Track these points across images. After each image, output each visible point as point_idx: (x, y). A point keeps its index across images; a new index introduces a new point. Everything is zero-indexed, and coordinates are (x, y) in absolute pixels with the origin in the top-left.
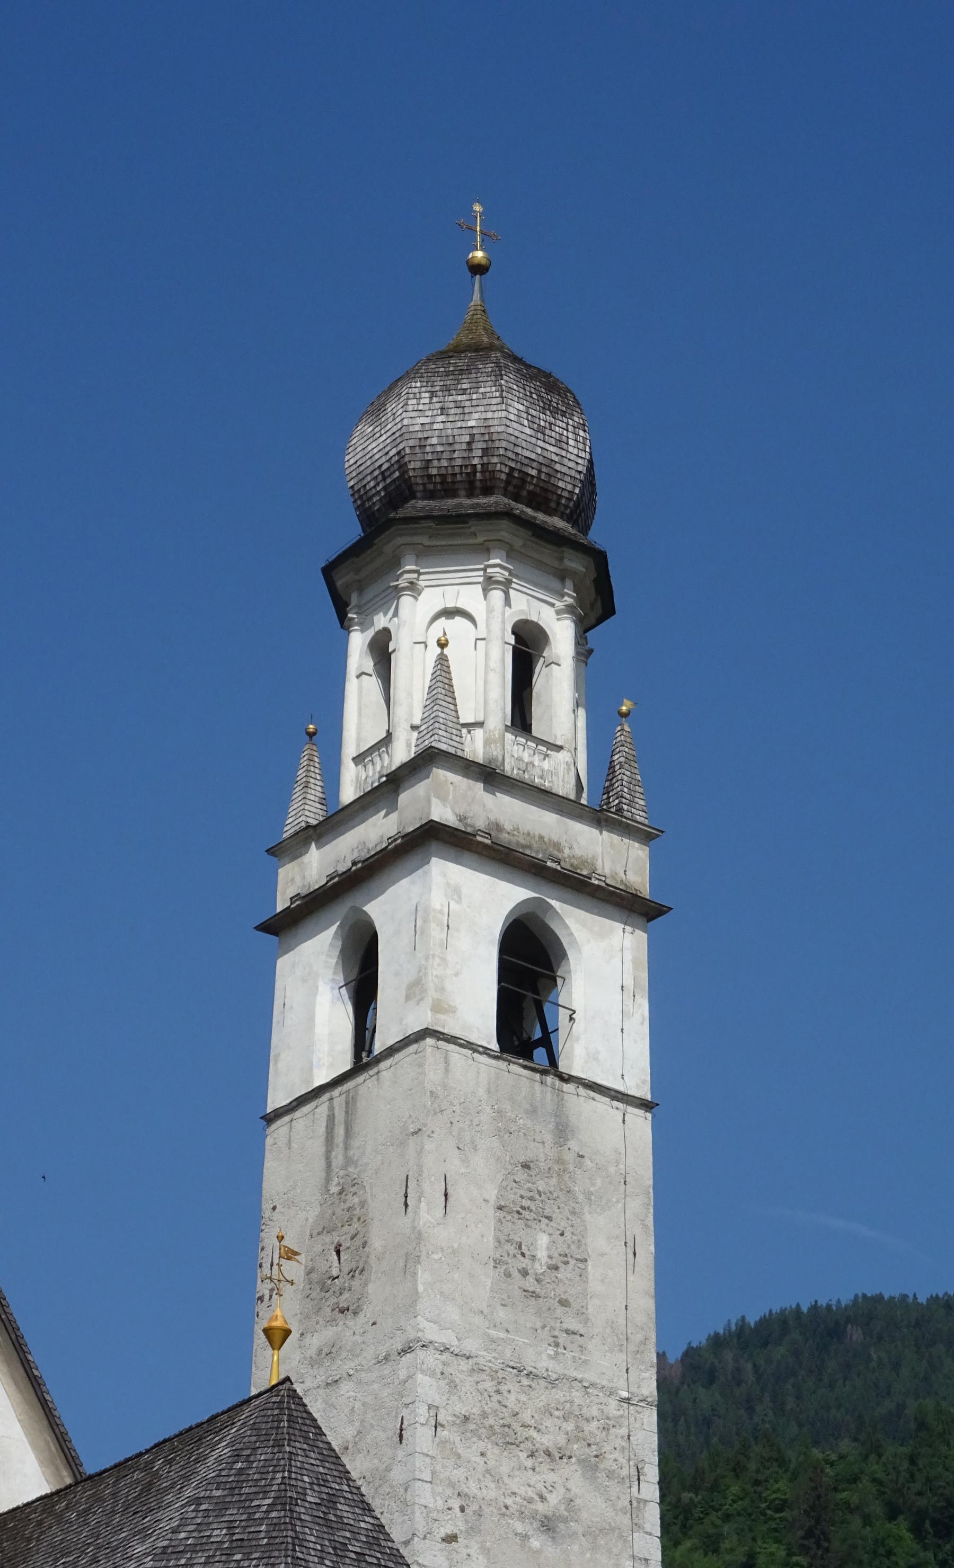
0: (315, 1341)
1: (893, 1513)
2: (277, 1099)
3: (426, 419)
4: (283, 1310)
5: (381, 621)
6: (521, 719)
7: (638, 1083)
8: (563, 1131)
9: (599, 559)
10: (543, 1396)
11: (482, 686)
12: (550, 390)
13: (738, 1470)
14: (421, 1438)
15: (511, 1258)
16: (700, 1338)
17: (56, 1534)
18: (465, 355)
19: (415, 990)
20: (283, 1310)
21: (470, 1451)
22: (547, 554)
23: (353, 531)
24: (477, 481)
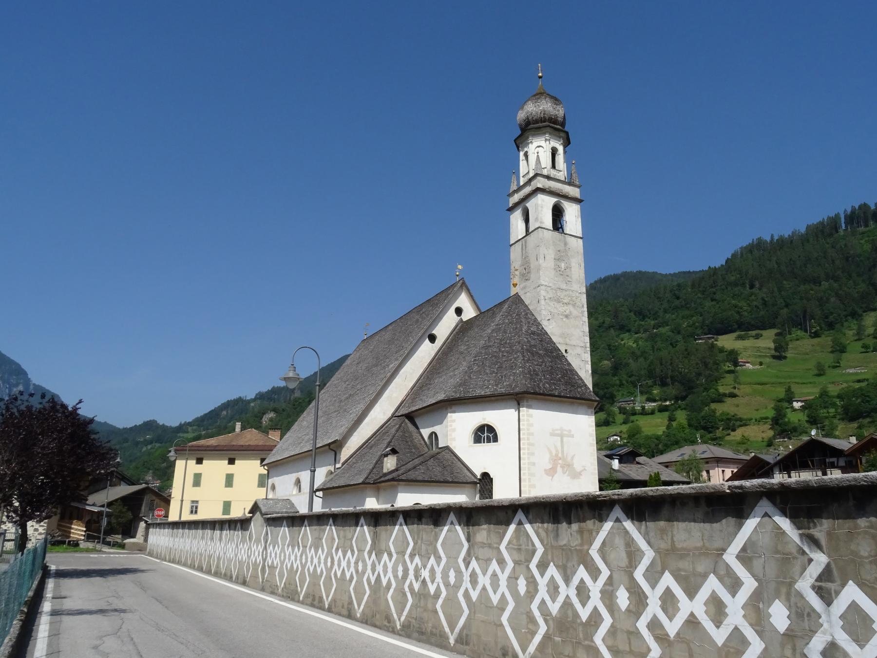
0: (522, 286)
1: (630, 311)
2: (512, 242)
3: (533, 108)
4: (516, 280)
5: (526, 149)
6: (554, 166)
7: (580, 234)
8: (566, 244)
9: (567, 133)
10: (565, 293)
11: (546, 161)
12: (556, 100)
13: (601, 305)
14: (542, 302)
15: (557, 269)
16: (592, 282)
17: (477, 323)
18: (539, 95)
19: (536, 219)
20: (516, 280)
21: (551, 304)
22: (557, 133)
23: (520, 132)
24: (542, 120)
